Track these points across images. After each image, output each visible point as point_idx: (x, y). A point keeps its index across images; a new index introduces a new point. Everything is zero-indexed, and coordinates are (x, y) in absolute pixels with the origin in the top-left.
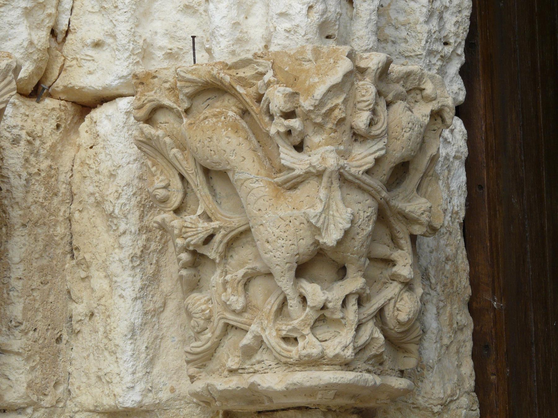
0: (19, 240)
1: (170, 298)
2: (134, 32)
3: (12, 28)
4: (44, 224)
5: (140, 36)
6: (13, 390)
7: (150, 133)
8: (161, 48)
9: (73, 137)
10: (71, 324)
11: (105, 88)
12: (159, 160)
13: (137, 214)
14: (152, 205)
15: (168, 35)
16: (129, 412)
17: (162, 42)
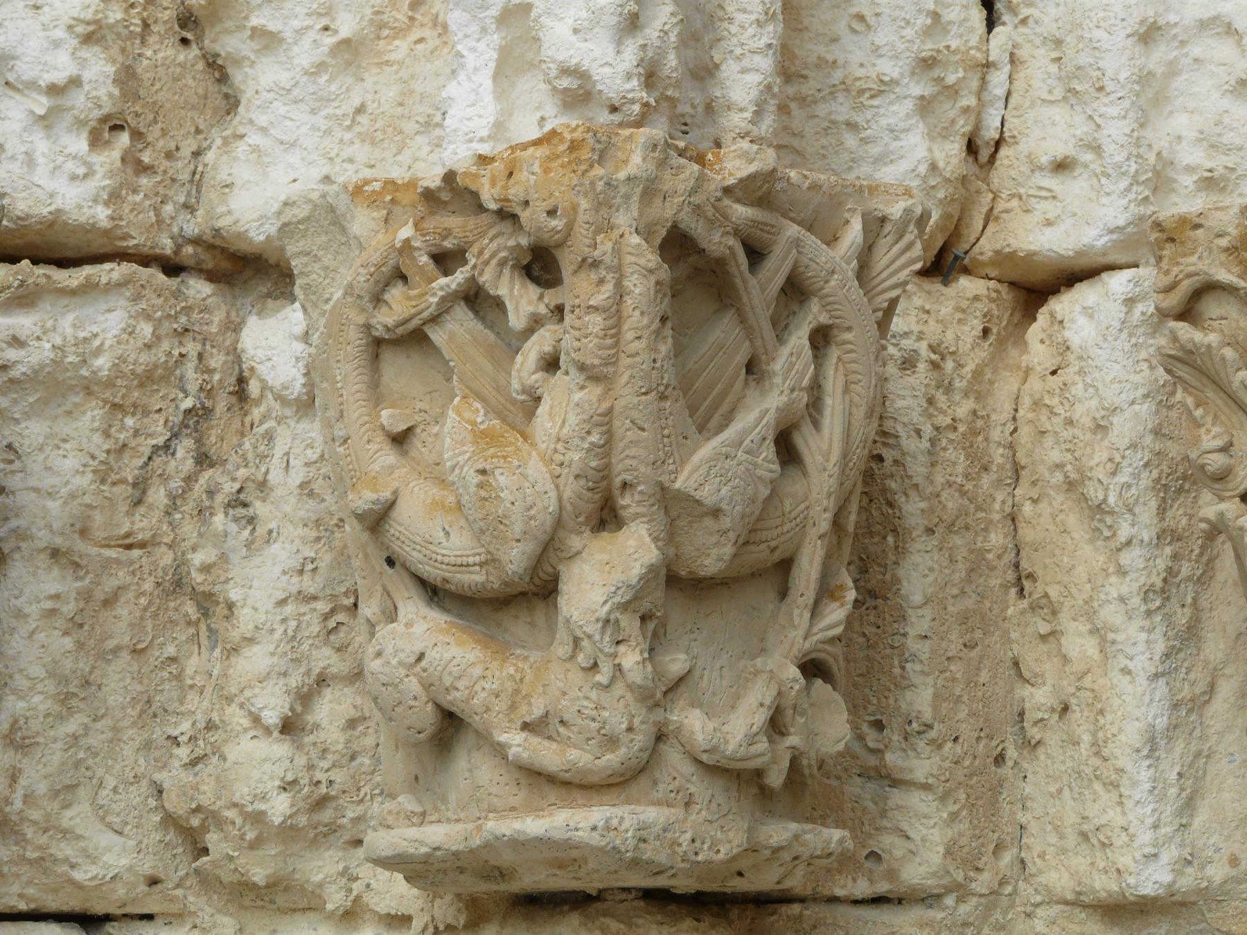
0: (920, 560)
1: (1223, 675)
2: (1138, 138)
3: (896, 139)
4: (967, 528)
5: (1150, 146)
6: (918, 860)
7: (1192, 340)
8: (1189, 169)
9: (1013, 353)
10: (1023, 728)
11: (1080, 253)
12: (1210, 393)
13: (1154, 504)
14: (1182, 486)
15: (1205, 143)
16: (1146, 904)
17: (1192, 155)
